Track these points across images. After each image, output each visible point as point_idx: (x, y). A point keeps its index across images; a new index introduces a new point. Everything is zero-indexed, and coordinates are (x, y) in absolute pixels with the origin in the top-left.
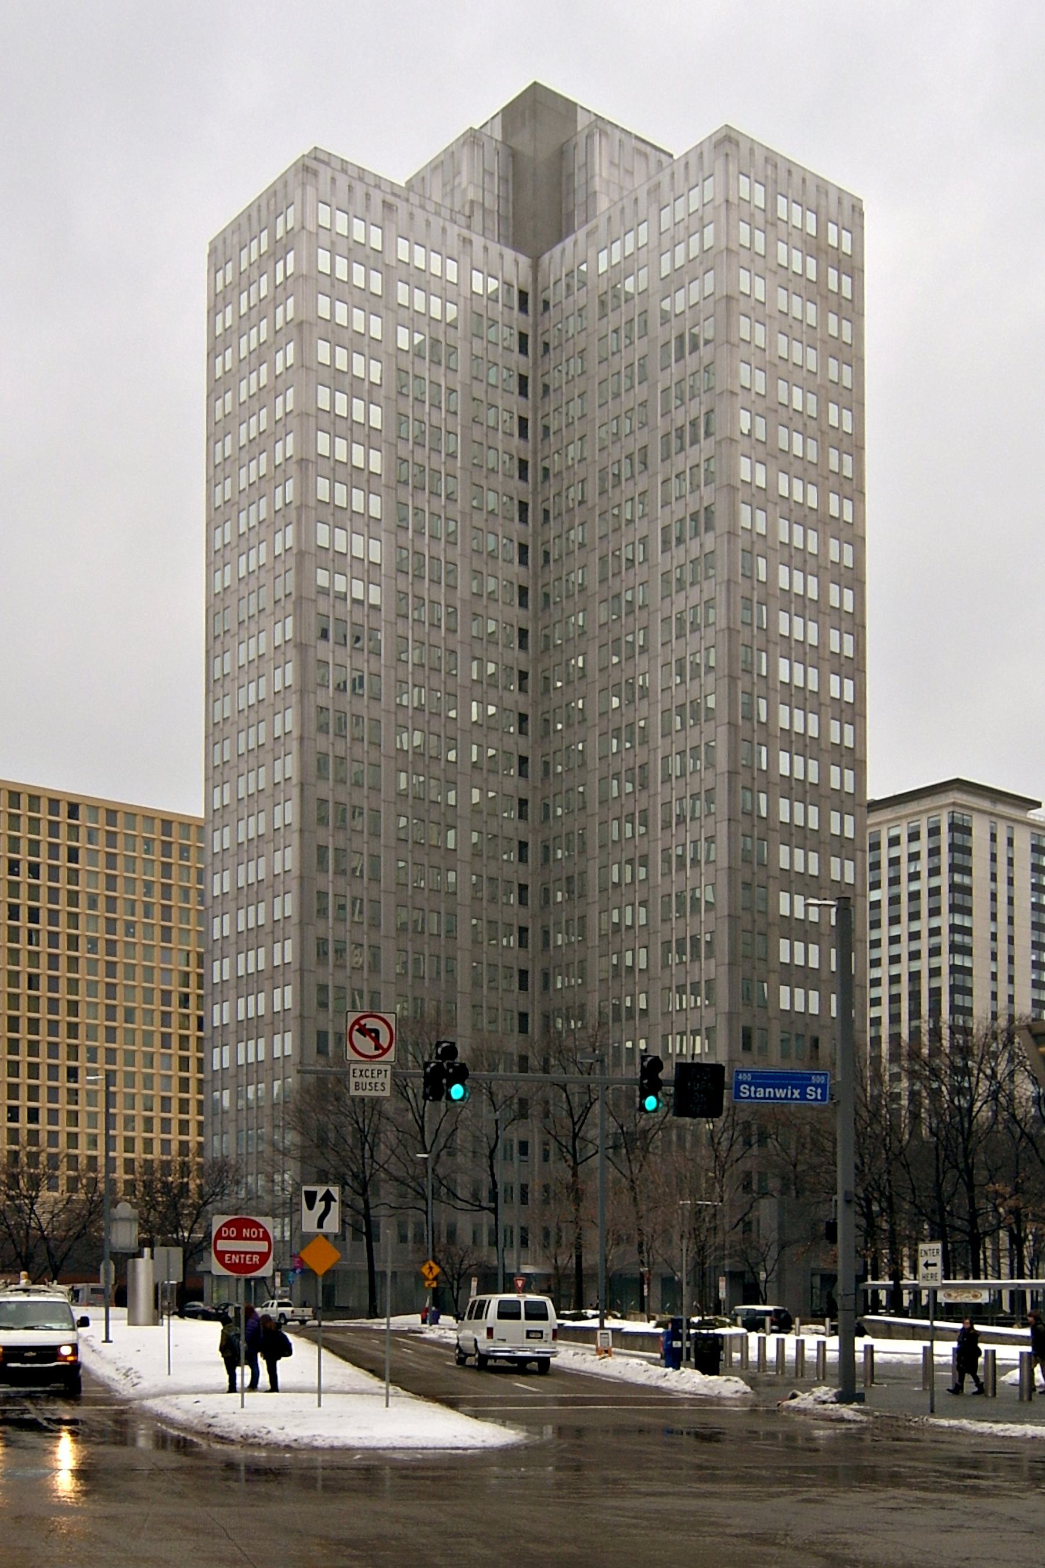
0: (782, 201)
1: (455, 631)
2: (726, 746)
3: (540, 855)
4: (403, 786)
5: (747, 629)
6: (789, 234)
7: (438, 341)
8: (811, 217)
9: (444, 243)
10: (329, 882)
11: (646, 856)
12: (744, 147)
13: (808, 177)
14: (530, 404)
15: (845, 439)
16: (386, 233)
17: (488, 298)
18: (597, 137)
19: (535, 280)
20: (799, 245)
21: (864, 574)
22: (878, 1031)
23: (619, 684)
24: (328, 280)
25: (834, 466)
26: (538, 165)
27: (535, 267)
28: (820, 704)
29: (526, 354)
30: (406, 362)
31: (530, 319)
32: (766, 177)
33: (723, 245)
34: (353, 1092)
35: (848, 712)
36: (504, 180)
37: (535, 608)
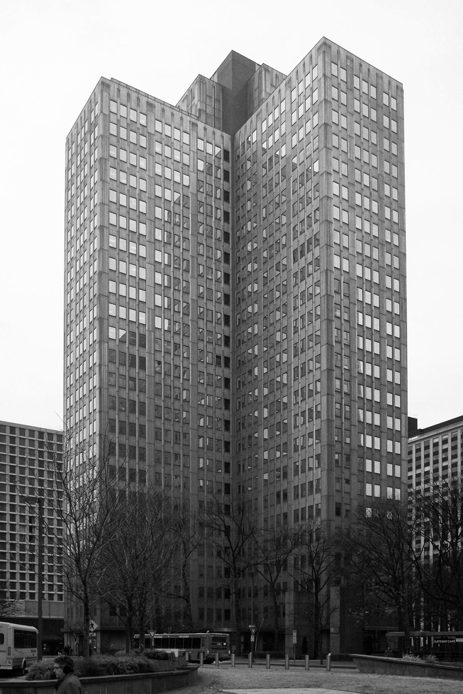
0: (356, 80)
4: (201, 465)
5: (337, 296)
6: (360, 96)
9: (182, 124)
10: (116, 438)
11: (286, 513)
12: (334, 49)
13: (371, 68)
14: (230, 205)
15: (394, 203)
16: (383, 440)
17: (174, 203)
18: (263, 72)
19: (233, 145)
20: (366, 102)
21: (406, 273)
22: (428, 553)
23: (280, 445)
24: (115, 139)
25: (389, 285)
27: (233, 140)
28: (381, 337)
29: (228, 182)
30: (201, 177)
31: (230, 165)
32: (347, 65)
33: (322, 98)
34: (36, 649)
35: (396, 343)
36: (217, 100)
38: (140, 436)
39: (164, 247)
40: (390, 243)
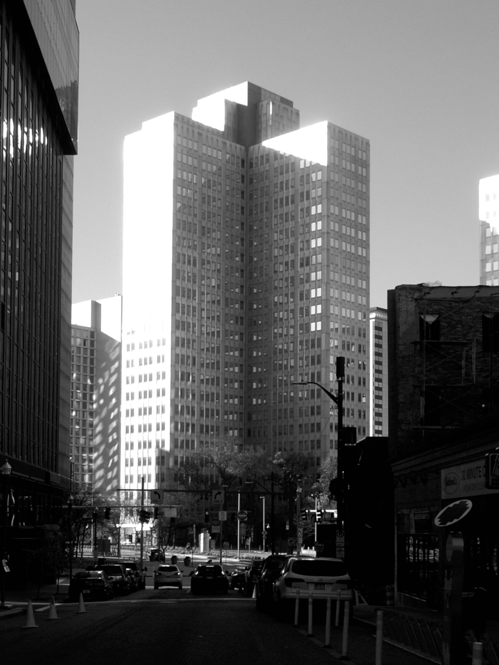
1: (221, 192)
3: (199, 414)
8: (353, 149)
38: (217, 352)
39: (207, 240)
40: (189, 172)
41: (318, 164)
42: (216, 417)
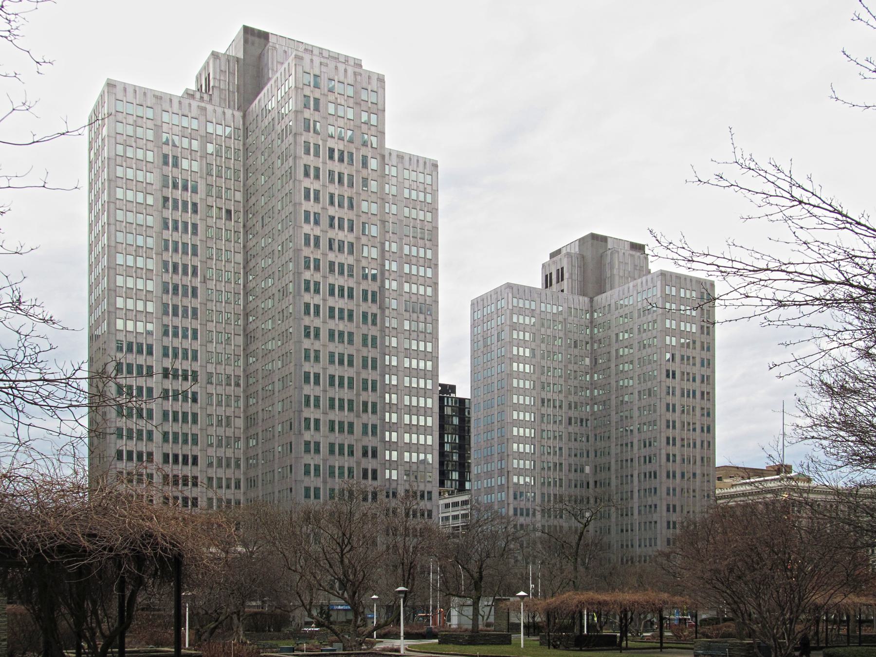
2: (438, 433)
7: (177, 157)
26: (593, 264)
37: (324, 316)
41: (366, 93)
42: (551, 480)
